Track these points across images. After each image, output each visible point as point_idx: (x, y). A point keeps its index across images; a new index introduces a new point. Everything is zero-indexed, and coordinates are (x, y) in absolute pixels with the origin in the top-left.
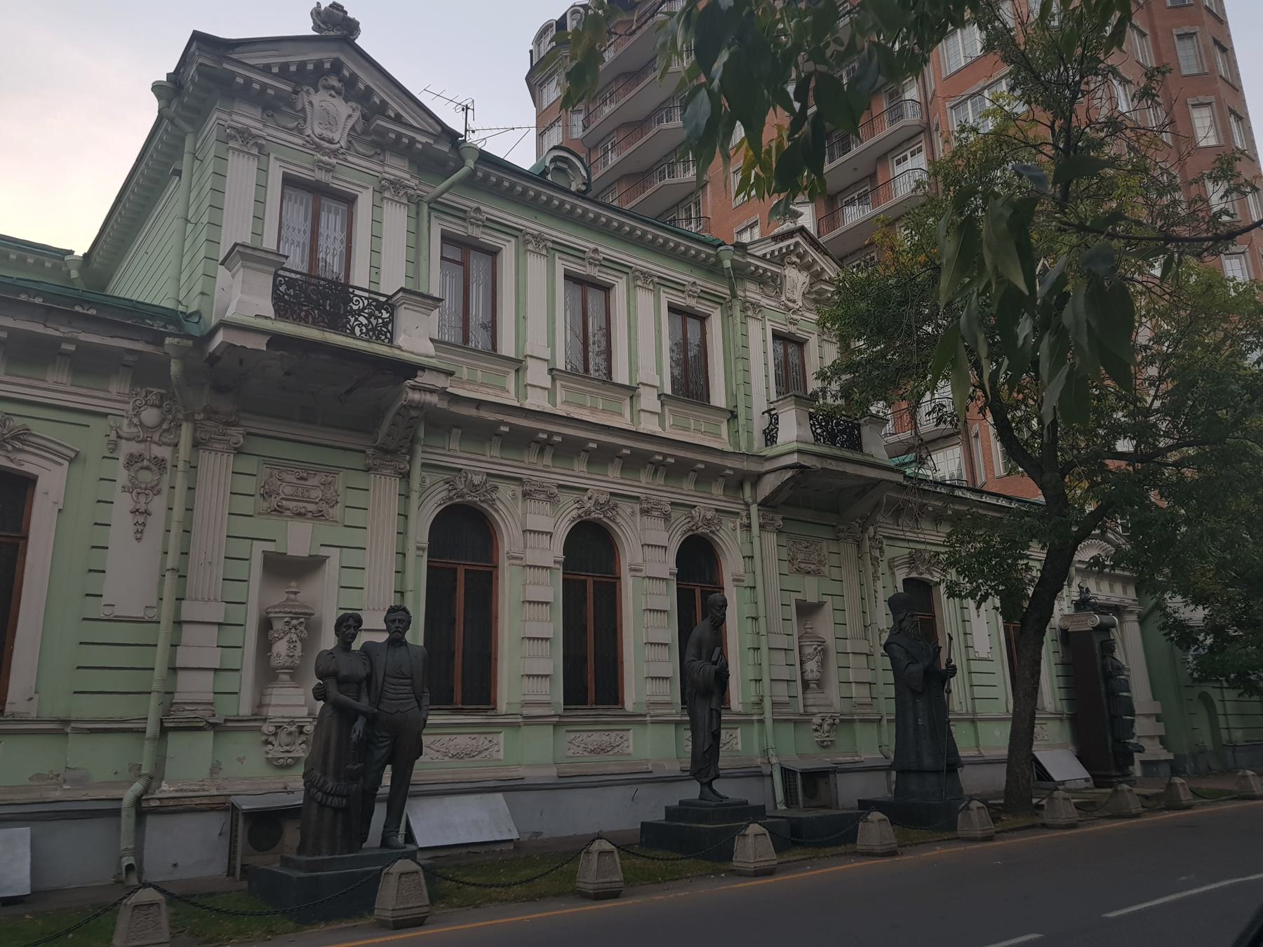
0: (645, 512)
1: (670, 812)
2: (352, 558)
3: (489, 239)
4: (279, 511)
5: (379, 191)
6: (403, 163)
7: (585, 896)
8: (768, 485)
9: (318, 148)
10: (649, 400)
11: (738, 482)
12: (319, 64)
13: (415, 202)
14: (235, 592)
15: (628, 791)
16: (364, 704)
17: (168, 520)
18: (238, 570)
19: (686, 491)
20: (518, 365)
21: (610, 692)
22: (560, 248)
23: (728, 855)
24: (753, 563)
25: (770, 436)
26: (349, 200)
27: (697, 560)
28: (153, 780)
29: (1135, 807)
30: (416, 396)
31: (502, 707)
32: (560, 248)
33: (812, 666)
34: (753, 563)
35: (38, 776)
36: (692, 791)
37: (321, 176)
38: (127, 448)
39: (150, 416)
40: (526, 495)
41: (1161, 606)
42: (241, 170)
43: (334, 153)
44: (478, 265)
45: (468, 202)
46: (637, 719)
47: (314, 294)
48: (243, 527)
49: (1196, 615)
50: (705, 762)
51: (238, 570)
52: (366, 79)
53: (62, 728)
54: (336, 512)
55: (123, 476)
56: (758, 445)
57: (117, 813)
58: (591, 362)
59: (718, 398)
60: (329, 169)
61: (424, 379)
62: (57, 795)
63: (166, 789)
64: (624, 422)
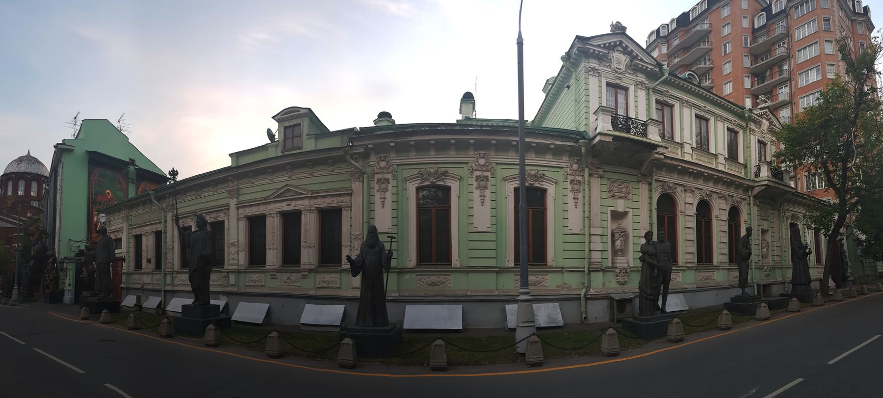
0: (720, 198)
1: (732, 299)
2: (636, 212)
3: (670, 101)
4: (614, 196)
5: (636, 85)
6: (643, 76)
7: (721, 329)
8: (756, 191)
9: (616, 72)
10: (721, 159)
11: (748, 189)
12: (615, 42)
13: (648, 89)
14: (604, 224)
15: (715, 292)
16: (655, 263)
17: (584, 201)
18: (604, 217)
19: (732, 191)
20: (681, 145)
21: (709, 259)
22: (693, 105)
23: (755, 313)
24: (749, 215)
25: (757, 174)
26: (626, 89)
27: (734, 213)
28: (588, 288)
29: (840, 296)
30: (657, 156)
31: (680, 264)
32: (693, 105)
33: (765, 250)
34: (749, 215)
35: (558, 286)
36: (738, 292)
37: (618, 81)
38: (570, 178)
39: (575, 167)
40: (685, 191)
41: (852, 233)
42: (593, 81)
43: (621, 73)
44: (667, 111)
45: (664, 89)
46: (717, 268)
47: (622, 123)
48: (605, 202)
49: (863, 237)
50: (743, 282)
51: (604, 217)
52: (631, 47)
53: (562, 270)
54: (630, 196)
55: (569, 187)
56: (753, 177)
57: (579, 299)
58: (703, 145)
59: (741, 160)
60: (620, 79)
61: (660, 150)
62: (563, 292)
63: (592, 291)
64: (714, 166)
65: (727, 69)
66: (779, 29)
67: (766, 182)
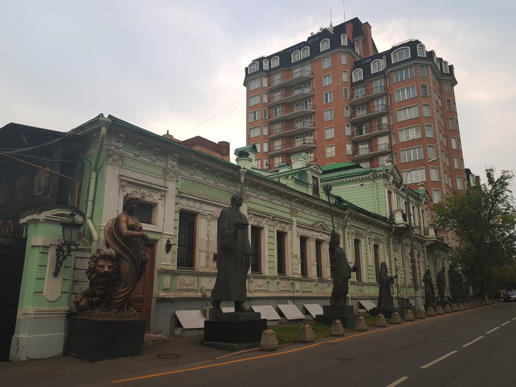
8: (427, 243)
11: (423, 242)
51: (272, 234)
65: (328, 115)
66: (378, 86)
67: (436, 239)
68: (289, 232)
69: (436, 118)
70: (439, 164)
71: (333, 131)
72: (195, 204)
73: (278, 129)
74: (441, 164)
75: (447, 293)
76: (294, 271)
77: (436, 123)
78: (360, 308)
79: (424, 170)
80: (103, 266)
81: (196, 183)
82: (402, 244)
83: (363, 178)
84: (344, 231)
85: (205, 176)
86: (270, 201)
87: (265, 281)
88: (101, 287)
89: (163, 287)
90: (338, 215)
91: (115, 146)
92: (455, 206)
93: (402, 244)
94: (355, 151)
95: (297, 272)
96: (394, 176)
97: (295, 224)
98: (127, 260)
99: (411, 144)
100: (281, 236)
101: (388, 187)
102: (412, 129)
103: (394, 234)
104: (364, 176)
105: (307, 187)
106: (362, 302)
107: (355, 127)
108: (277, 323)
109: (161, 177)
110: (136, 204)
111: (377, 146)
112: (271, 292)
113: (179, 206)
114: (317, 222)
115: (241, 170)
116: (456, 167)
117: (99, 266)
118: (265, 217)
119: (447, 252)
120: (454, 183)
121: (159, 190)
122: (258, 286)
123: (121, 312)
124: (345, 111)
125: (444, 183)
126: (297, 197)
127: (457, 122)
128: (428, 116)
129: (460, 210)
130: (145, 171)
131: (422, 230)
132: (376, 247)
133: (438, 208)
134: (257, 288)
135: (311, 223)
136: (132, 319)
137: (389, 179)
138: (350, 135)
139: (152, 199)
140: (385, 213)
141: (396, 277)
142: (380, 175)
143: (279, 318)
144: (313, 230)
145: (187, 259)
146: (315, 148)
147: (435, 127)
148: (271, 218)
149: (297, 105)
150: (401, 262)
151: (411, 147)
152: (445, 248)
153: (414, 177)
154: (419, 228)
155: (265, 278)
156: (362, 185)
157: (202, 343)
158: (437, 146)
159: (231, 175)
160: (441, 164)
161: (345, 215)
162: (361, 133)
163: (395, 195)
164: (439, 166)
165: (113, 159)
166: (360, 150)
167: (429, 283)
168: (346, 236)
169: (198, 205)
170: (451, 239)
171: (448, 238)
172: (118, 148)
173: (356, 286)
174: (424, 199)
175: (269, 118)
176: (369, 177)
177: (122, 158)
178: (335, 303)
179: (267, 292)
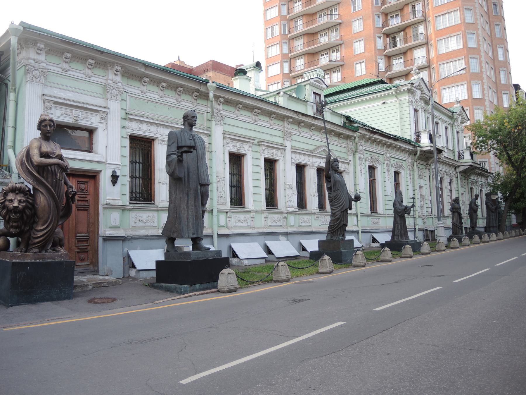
8: (461, 169)
51: (257, 162)
67: (471, 164)
68: (281, 159)
69: (479, 25)
70: (482, 79)
71: (363, 45)
72: (149, 128)
73: (300, 45)
74: (485, 78)
75: (481, 223)
76: (288, 204)
77: (480, 30)
78: (373, 242)
79: (465, 86)
80: (12, 201)
81: (150, 103)
82: (429, 169)
83: (385, 95)
84: (354, 156)
85: (161, 93)
86: (255, 123)
87: (249, 216)
88: (14, 224)
89: (109, 223)
90: (347, 137)
91: (34, 60)
92: (495, 124)
93: (429, 169)
94: (389, 67)
95: (291, 204)
96: (422, 91)
97: (288, 149)
98: (42, 193)
99: (451, 56)
100: (270, 164)
101: (414, 104)
102: (452, 38)
103: (420, 158)
104: (386, 93)
105: (306, 106)
106: (375, 236)
107: (388, 39)
108: (264, 261)
109: (101, 96)
110: (50, 126)
111: (412, 59)
112: (258, 228)
113: (128, 130)
114: (319, 147)
115: (208, 84)
116: (503, 82)
117: (8, 200)
118: (247, 142)
119: (487, 177)
120: (500, 99)
121: (98, 111)
122: (240, 221)
123: (43, 252)
124: (376, 20)
125: (487, 101)
126: (291, 117)
127: (505, 29)
128: (471, 22)
129: (500, 130)
130: (241, 123)
131: (457, 154)
132: (397, 174)
133: (476, 129)
134: (237, 224)
135: (311, 148)
136: (57, 260)
137: (415, 95)
138: (382, 48)
139: (89, 123)
140: (409, 135)
141: (413, 206)
142: (404, 90)
143: (265, 255)
144: (313, 156)
145: (143, 193)
146: (342, 65)
147: (478, 35)
148: (255, 142)
149: (321, 16)
150: (428, 190)
151: (451, 60)
152: (483, 172)
153: (451, 96)
154: (453, 151)
155: (249, 212)
156: (384, 103)
157: (152, 286)
158: (480, 57)
159: (198, 91)
160: (485, 78)
161: (355, 137)
162: (395, 45)
163: (423, 113)
164: (482, 81)
165: (33, 75)
166: (394, 66)
167: (457, 212)
168: (358, 162)
169: (153, 129)
170: (494, 164)
171: (490, 163)
172: (38, 62)
173: (369, 218)
174: (460, 118)
175: (289, 32)
176: (392, 93)
177: (45, 73)
178: (332, 237)
179: (252, 227)
